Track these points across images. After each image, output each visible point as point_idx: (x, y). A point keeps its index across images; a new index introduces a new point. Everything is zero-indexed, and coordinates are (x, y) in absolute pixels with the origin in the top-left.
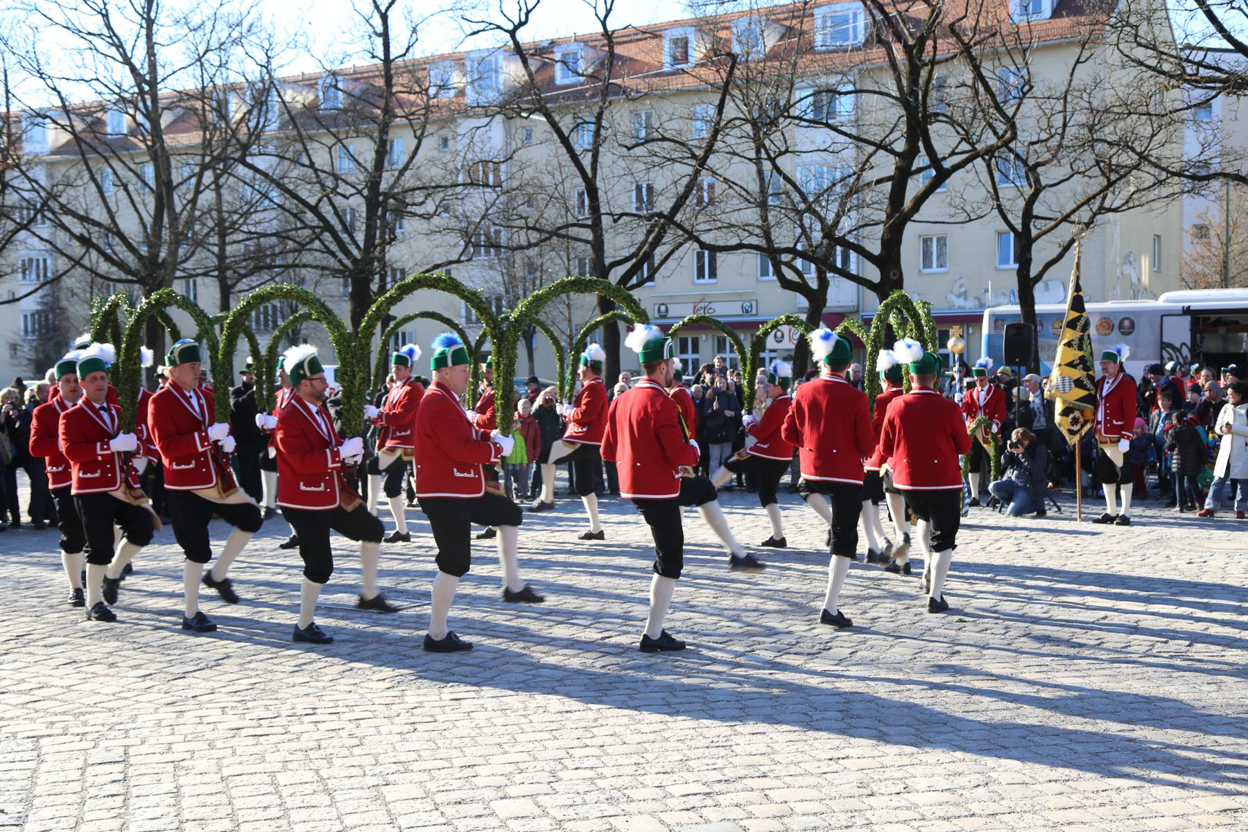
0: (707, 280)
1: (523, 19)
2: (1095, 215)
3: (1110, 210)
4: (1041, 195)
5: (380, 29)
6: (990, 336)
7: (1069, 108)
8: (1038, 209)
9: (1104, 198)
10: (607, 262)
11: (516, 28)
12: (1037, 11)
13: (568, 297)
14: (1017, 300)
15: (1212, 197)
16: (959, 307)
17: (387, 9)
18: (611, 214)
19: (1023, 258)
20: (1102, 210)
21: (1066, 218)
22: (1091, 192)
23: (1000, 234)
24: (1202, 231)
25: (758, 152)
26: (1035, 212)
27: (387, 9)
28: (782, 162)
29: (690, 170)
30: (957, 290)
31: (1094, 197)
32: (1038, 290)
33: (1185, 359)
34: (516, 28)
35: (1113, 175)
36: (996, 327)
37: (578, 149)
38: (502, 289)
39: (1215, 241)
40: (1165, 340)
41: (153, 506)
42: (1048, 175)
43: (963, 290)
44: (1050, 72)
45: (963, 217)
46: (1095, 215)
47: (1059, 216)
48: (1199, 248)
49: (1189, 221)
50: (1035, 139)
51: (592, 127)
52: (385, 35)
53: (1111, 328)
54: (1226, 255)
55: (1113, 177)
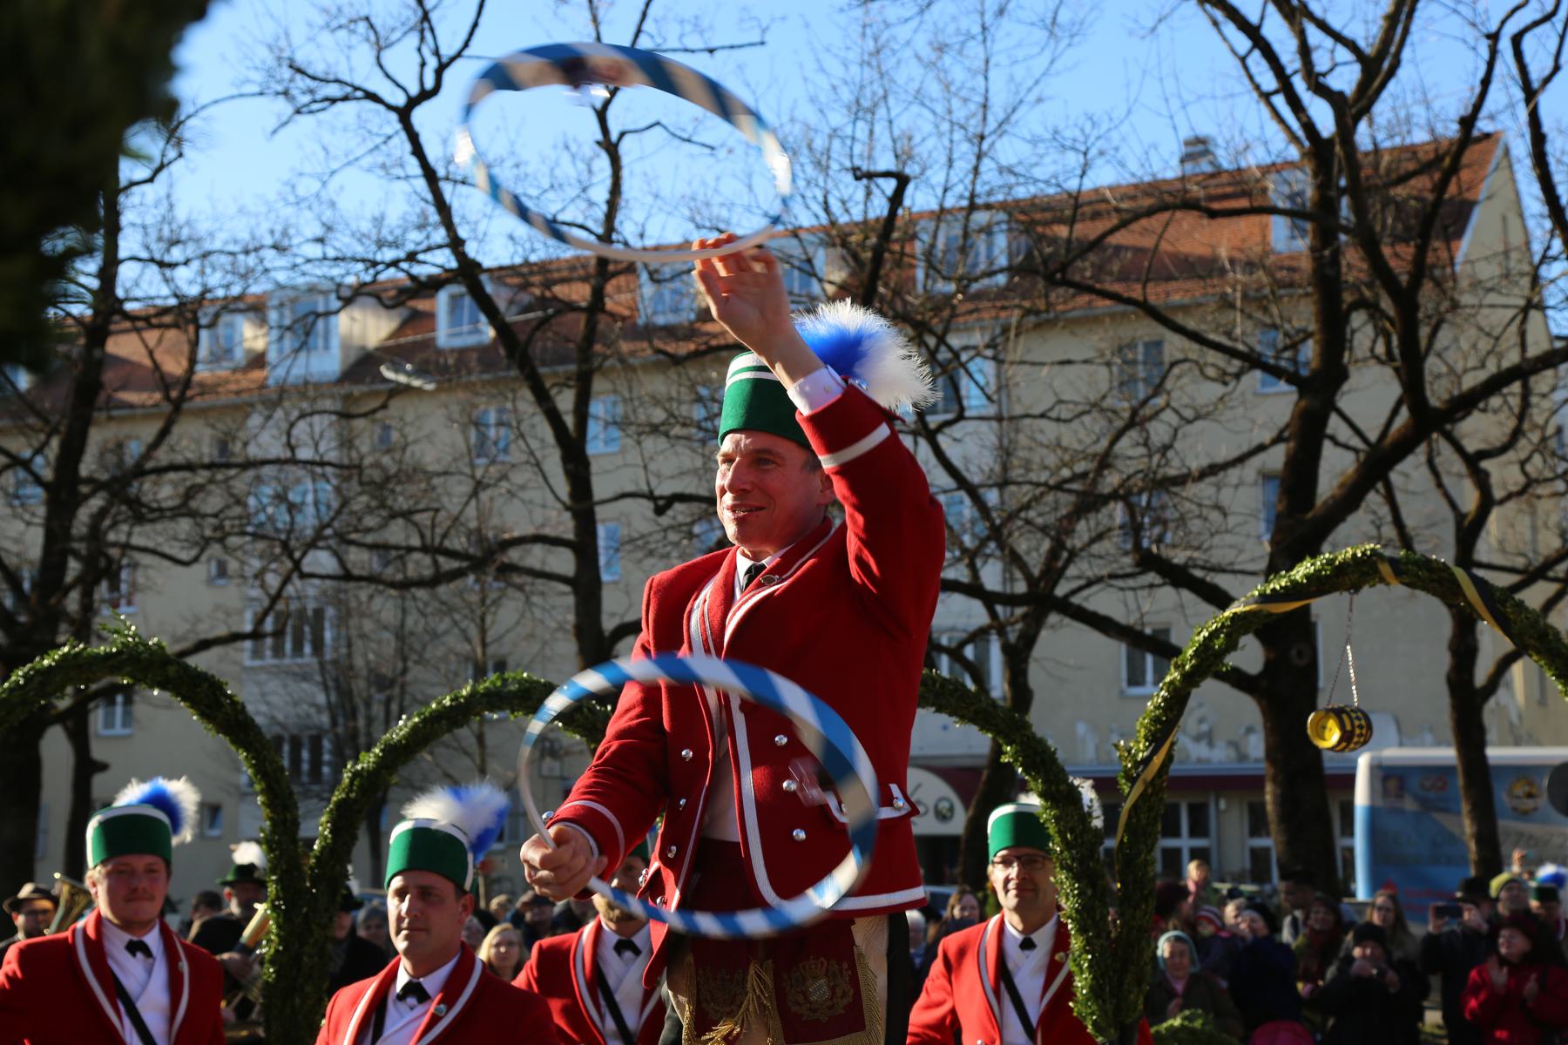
1: (429, 83)
6: (1373, 812)
10: (609, 624)
11: (413, 102)
13: (1364, 324)
14: (1449, 734)
16: (1199, 761)
18: (650, 496)
34: (413, 102)
38: (325, 719)
43: (1205, 727)
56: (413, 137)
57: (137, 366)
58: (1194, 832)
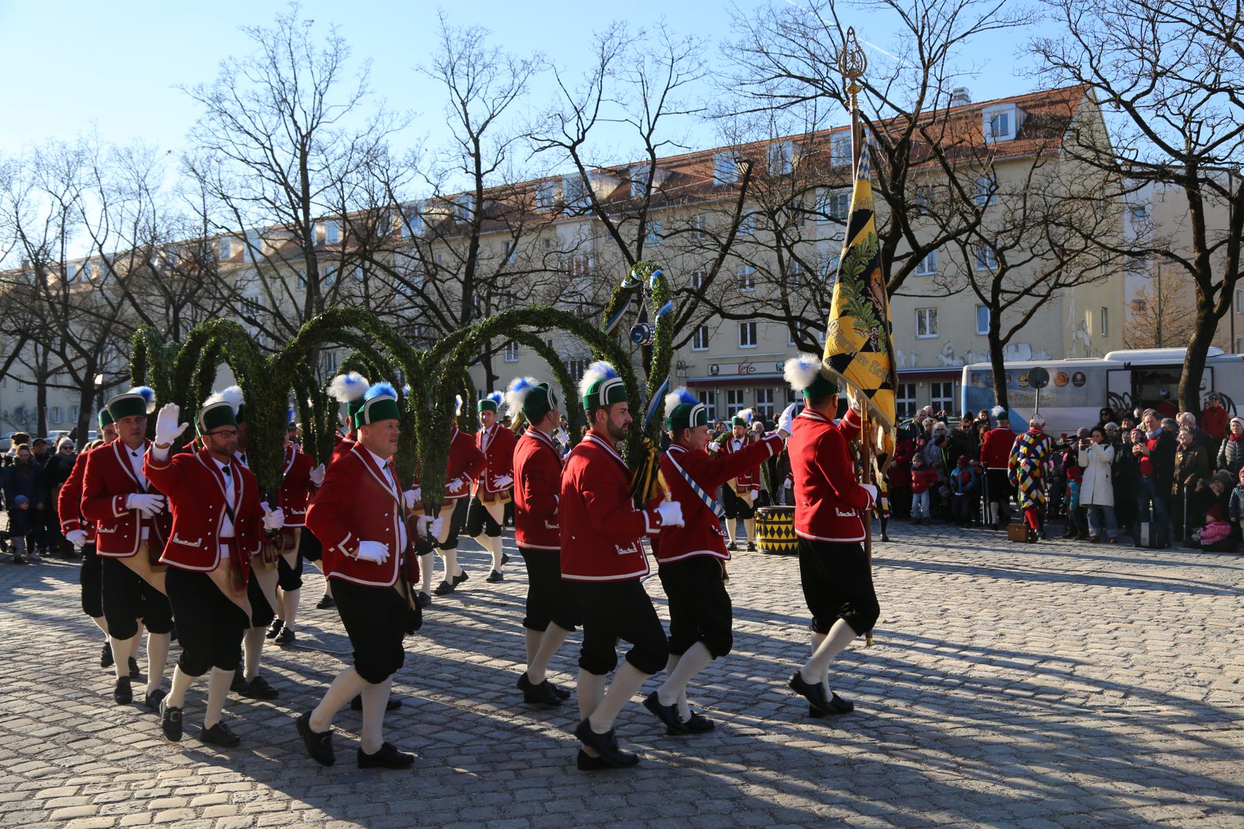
0: (749, 346)
2: (1051, 289)
3: (1063, 285)
4: (1007, 274)
5: (473, 151)
6: (967, 388)
7: (1028, 205)
8: (1004, 284)
9: (1059, 275)
11: (575, 144)
12: (1005, 133)
15: (1146, 274)
17: (479, 134)
19: (995, 326)
20: (1057, 285)
21: (1027, 291)
22: (1047, 271)
23: (979, 307)
24: (1140, 305)
25: (778, 242)
26: (1003, 287)
27: (479, 134)
28: (797, 249)
29: (716, 255)
30: (945, 351)
31: (1050, 274)
32: (1007, 351)
33: (1127, 405)
34: (575, 144)
35: (1064, 255)
36: (973, 380)
37: (627, 241)
39: (1150, 312)
40: (1111, 390)
41: (955, 467)
42: (1011, 257)
44: (1012, 177)
45: (944, 291)
46: (1051, 289)
47: (1022, 290)
48: (1139, 319)
49: (1130, 297)
50: (1001, 229)
51: (638, 222)
52: (477, 156)
53: (1066, 380)
54: (1159, 323)
55: (1066, 259)
56: (576, 157)
57: (544, 344)
58: (910, 397)
